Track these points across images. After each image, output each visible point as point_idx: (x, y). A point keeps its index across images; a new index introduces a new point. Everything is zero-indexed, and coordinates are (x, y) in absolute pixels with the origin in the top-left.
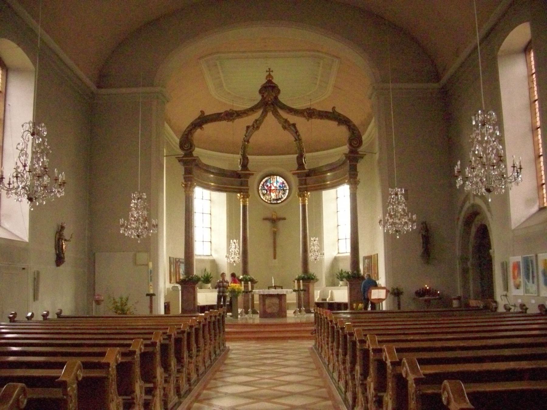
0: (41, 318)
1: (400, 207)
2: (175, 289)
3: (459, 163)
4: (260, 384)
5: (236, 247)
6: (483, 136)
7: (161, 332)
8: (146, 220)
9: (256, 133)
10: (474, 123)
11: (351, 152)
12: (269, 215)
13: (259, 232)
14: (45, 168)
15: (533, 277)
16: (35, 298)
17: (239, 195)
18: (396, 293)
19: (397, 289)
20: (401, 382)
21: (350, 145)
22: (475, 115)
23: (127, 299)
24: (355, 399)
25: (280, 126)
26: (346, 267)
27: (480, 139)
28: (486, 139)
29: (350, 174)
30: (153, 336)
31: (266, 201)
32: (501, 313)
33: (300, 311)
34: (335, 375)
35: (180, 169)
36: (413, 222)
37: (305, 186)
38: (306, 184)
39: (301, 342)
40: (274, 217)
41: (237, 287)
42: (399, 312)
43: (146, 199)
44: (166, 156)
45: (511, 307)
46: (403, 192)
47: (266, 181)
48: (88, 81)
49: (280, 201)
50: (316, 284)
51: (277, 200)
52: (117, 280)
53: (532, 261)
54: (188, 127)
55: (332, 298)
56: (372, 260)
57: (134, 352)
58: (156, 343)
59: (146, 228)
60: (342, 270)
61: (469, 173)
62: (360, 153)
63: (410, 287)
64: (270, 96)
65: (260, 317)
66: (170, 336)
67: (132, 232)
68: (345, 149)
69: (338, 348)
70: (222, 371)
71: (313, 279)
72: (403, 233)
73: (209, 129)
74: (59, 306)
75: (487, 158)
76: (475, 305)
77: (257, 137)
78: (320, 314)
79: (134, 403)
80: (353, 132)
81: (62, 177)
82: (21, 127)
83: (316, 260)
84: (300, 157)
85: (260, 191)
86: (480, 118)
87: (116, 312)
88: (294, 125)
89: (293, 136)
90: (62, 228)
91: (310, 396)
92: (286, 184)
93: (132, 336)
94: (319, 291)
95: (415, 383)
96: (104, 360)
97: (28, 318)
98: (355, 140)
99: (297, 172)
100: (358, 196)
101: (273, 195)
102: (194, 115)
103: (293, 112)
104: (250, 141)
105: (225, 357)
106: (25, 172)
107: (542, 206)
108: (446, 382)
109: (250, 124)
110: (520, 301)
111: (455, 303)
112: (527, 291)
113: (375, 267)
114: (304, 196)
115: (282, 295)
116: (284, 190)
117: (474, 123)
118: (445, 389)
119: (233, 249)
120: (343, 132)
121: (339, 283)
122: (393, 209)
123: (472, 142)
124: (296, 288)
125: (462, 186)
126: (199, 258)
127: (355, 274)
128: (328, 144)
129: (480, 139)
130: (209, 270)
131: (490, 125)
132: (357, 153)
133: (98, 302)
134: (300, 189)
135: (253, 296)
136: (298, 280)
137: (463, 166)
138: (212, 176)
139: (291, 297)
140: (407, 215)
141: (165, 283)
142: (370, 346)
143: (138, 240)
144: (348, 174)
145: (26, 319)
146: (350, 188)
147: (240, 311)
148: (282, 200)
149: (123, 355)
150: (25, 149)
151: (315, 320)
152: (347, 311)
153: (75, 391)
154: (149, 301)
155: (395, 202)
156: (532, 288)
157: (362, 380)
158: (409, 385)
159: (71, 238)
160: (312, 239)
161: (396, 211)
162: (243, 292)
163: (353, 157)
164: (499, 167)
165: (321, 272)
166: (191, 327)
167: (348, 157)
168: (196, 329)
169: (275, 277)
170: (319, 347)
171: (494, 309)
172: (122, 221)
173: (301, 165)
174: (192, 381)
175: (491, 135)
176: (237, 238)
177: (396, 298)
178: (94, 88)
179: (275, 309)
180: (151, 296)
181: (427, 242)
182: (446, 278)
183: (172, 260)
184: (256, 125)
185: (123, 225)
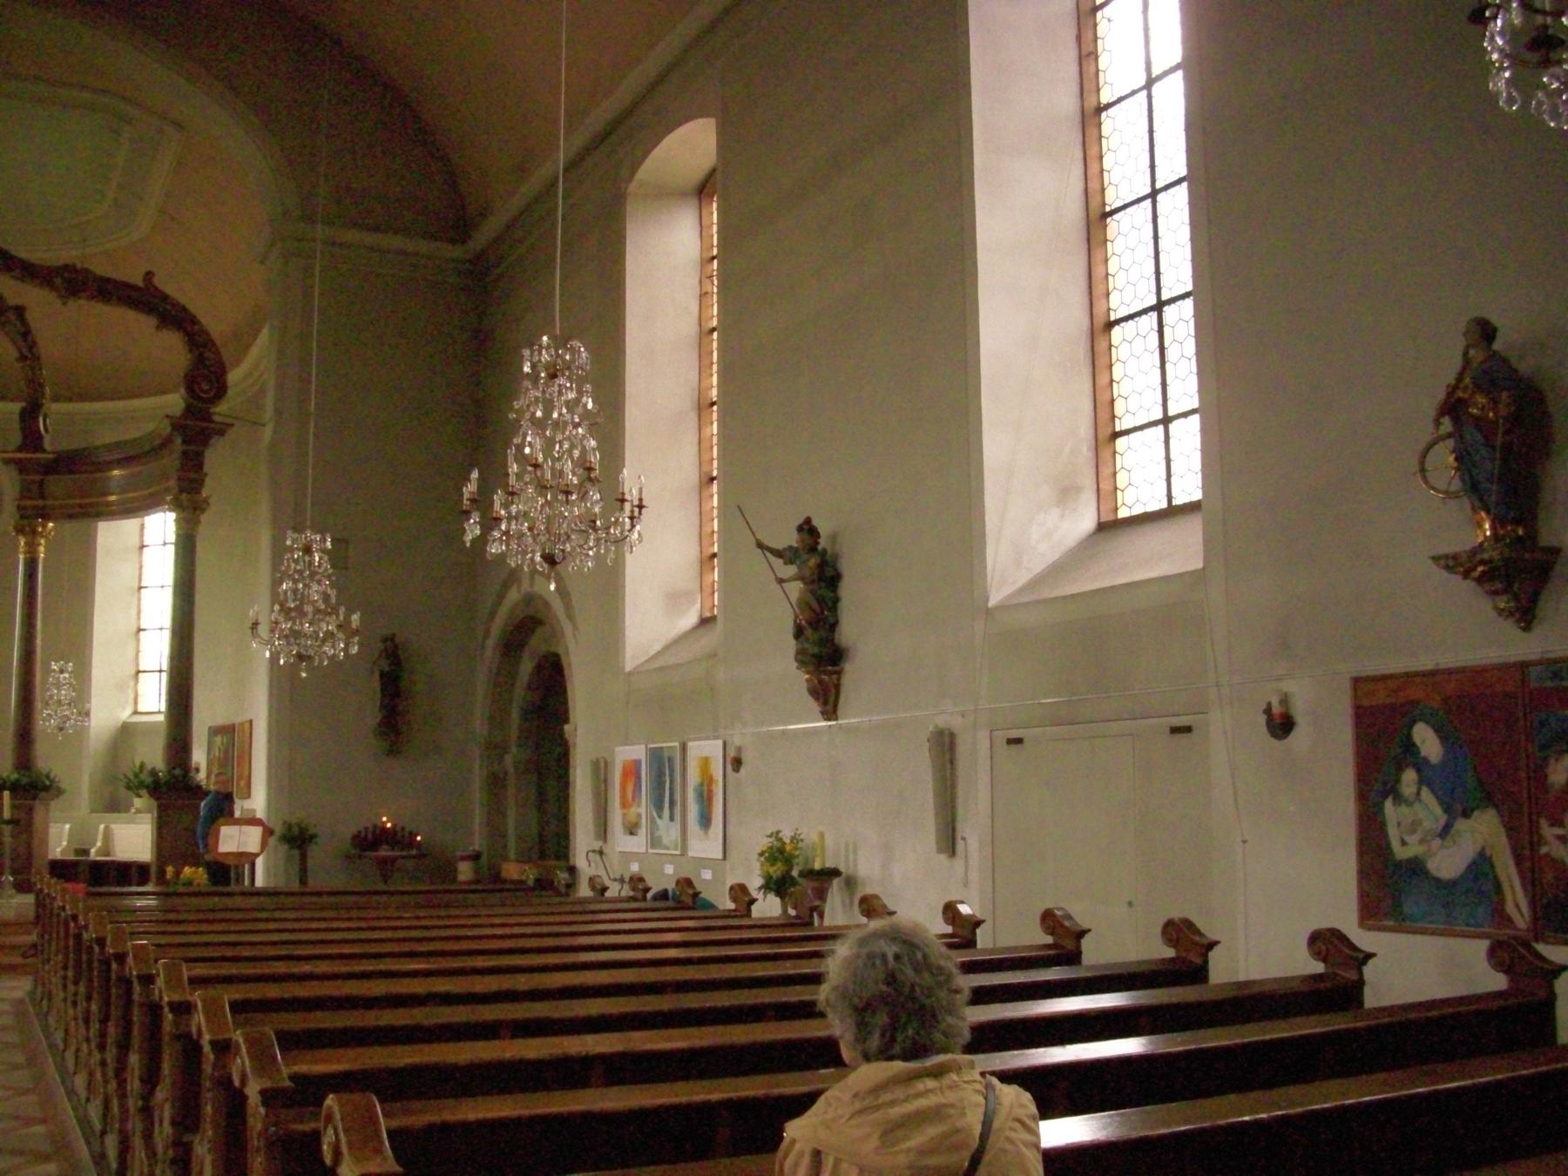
1: (315, 587)
3: (475, 475)
6: (549, 407)
10: (527, 369)
11: (189, 411)
15: (672, 803)
18: (296, 840)
19: (299, 825)
20: (235, 1102)
21: (190, 389)
22: (531, 346)
26: (153, 756)
27: (539, 414)
28: (555, 415)
32: (582, 901)
34: (80, 1082)
37: (40, 503)
38: (43, 497)
42: (303, 894)
45: (607, 883)
46: (329, 545)
53: (670, 760)
55: (106, 850)
56: (232, 737)
60: (142, 766)
62: (217, 418)
63: (338, 825)
68: (175, 402)
69: (89, 998)
71: (46, 789)
72: (321, 662)
75: (553, 468)
76: (515, 877)
80: (201, 355)
83: (61, 729)
84: (31, 413)
86: (545, 357)
89: (14, 342)
95: (265, 1103)
98: (206, 376)
99: (19, 455)
103: (17, 273)
107: (708, 614)
108: (330, 1100)
110: (635, 868)
111: (465, 871)
112: (655, 841)
113: (241, 758)
114: (34, 532)
117: (527, 369)
118: (329, 1118)
120: (171, 351)
121: (132, 805)
122: (295, 591)
123: (518, 421)
125: (482, 541)
127: (175, 777)
129: (539, 414)
131: (570, 379)
132: (207, 418)
134: (23, 513)
140: (335, 611)
142: (164, 992)
146: (177, 521)
155: (301, 572)
156: (669, 832)
157: (143, 1098)
158: (250, 1111)
161: (303, 599)
163: (196, 431)
164: (584, 496)
165: (77, 772)
167: (178, 426)
171: (563, 890)
173: (32, 439)
175: (572, 406)
177: (296, 852)
181: (396, 694)
182: (443, 798)
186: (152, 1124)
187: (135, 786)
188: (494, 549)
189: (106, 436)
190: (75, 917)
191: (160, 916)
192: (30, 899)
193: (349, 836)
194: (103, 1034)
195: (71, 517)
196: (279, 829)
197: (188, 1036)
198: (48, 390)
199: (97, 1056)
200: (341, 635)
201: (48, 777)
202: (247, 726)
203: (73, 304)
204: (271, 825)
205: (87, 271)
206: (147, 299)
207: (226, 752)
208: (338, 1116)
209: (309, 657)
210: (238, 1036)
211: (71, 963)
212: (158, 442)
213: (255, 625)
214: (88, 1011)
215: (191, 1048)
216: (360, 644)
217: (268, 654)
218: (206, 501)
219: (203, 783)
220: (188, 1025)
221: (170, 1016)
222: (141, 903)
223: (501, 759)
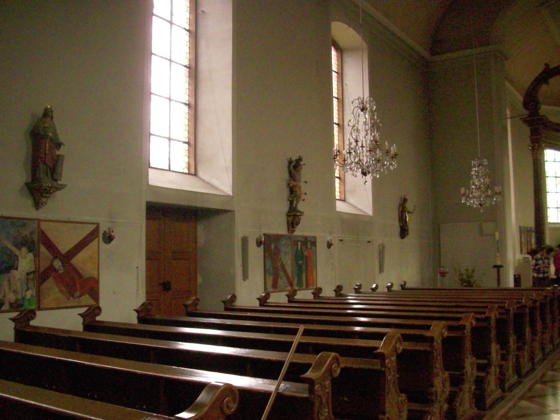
0: (386, 290)
2: (525, 260)
7: (496, 305)
8: (488, 187)
14: (376, 142)
16: (381, 270)
23: (473, 271)
30: (487, 311)
35: (526, 130)
48: (418, 48)
57: (464, 326)
58: (490, 317)
66: (508, 311)
74: (405, 279)
79: (464, 380)
81: (393, 149)
82: (351, 103)
90: (405, 200)
93: (464, 310)
96: (427, 334)
97: (373, 290)
106: (357, 148)
126: (553, 226)
133: (443, 274)
141: (514, 254)
143: (480, 209)
145: (371, 291)
149: (450, 328)
150: (356, 125)
153: (394, 364)
154: (496, 274)
159: (414, 210)
166: (535, 301)
172: (463, 190)
174: (536, 360)
178: (426, 54)
180: (498, 267)
183: (522, 228)
185: (464, 195)
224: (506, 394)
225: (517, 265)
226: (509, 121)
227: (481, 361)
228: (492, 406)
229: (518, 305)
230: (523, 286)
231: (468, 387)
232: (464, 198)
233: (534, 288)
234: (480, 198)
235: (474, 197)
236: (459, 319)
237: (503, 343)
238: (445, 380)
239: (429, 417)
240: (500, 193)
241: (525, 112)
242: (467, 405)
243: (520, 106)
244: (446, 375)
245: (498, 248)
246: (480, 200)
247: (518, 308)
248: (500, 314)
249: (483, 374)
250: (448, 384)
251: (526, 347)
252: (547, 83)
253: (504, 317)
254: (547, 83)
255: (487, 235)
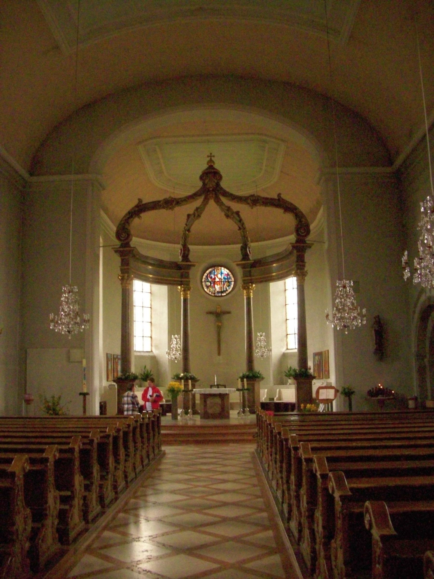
1: (348, 300)
3: (406, 253)
4: (192, 492)
5: (177, 342)
9: (196, 222)
10: (422, 210)
11: (297, 242)
12: (213, 309)
13: (201, 328)
17: (179, 287)
19: (348, 389)
20: (330, 499)
22: (423, 201)
23: (60, 398)
24: (290, 511)
25: (223, 214)
26: (294, 364)
27: (429, 227)
29: (297, 265)
30: (71, 440)
31: (210, 293)
33: (244, 412)
34: (274, 483)
35: (117, 259)
36: (362, 316)
37: (250, 278)
38: (250, 276)
39: (241, 446)
40: (219, 310)
41: (177, 386)
43: (77, 292)
44: (103, 247)
46: (352, 284)
47: (210, 273)
49: (225, 294)
50: (262, 383)
51: (222, 292)
52: (49, 378)
54: (125, 217)
55: (280, 398)
56: (321, 356)
58: (74, 449)
59: (78, 323)
60: (290, 368)
61: (417, 264)
63: (362, 388)
64: (211, 184)
65: (201, 418)
66: (92, 441)
67: (62, 328)
68: (292, 238)
69: (276, 454)
70: (152, 478)
71: (258, 377)
72: (352, 327)
73: (147, 217)
77: (197, 226)
78: (261, 416)
79: (46, 515)
84: (244, 248)
85: (203, 283)
87: (48, 413)
88: (238, 213)
91: (247, 507)
92: (231, 276)
94: (266, 390)
98: (302, 228)
100: (305, 288)
101: (217, 287)
102: (132, 204)
104: (191, 230)
105: (159, 462)
109: (191, 212)
111: (411, 404)
114: (248, 288)
115: (224, 394)
116: (229, 282)
117: (422, 210)
118: (367, 511)
119: (174, 345)
120: (289, 220)
121: (288, 382)
124: (240, 387)
125: (410, 279)
126: (138, 354)
127: (303, 372)
128: (274, 234)
129: (429, 227)
130: (148, 368)
132: (304, 242)
135: (194, 396)
136: (242, 379)
137: (411, 257)
138: (150, 267)
139: (235, 397)
141: (101, 381)
143: (68, 336)
144: (295, 264)
146: (297, 280)
147: (180, 411)
148: (227, 292)
149: (32, 461)
151: (257, 422)
152: (295, 413)
155: (343, 295)
158: (336, 503)
160: (259, 334)
161: (344, 305)
162: (183, 391)
163: (300, 248)
166: (118, 430)
168: (124, 432)
169: (219, 376)
170: (259, 451)
172: (51, 316)
173: (245, 256)
176: (178, 334)
178: (26, 175)
179: (218, 410)
180: (85, 395)
181: (381, 338)
183: (109, 355)
184: (197, 214)
185: (52, 321)
186: (300, 502)
187: (289, 376)
188: (416, 281)
189: (269, 253)
190: (270, 424)
191: (299, 423)
192: (254, 416)
193: (367, 392)
194: (281, 467)
195: (261, 282)
196: (340, 390)
197: (311, 471)
198: (249, 239)
199: (279, 475)
200: (359, 317)
201: (258, 373)
202: (327, 352)
203: (255, 209)
204: (338, 388)
205: (259, 196)
206: (279, 203)
207: (320, 362)
208: (371, 510)
209: (348, 326)
210: (331, 474)
211: (269, 440)
212: (288, 253)
213: (327, 316)
214: (276, 458)
215: (313, 476)
216: (367, 321)
217: (333, 326)
218: (306, 272)
219: (312, 374)
220: (312, 467)
221: (305, 463)
222: (293, 418)
223: (423, 359)
224: (90, 525)
225: (103, 392)
226: (101, 249)
227: (63, 493)
228: (75, 540)
229: (102, 434)
230: (108, 415)
231: (51, 522)
232: (52, 324)
233: (118, 416)
234: (68, 325)
235: (63, 324)
236: (42, 451)
237: (87, 473)
238: (27, 517)
239: (10, 559)
240: (88, 321)
241: (118, 243)
242: (49, 541)
243: (113, 235)
244: (28, 512)
245: (85, 375)
246: (69, 327)
247: (101, 437)
248: (84, 444)
249: (67, 507)
250: (30, 521)
251: (110, 476)
252: (140, 217)
253: (88, 447)
254: (140, 217)
255: (74, 362)
